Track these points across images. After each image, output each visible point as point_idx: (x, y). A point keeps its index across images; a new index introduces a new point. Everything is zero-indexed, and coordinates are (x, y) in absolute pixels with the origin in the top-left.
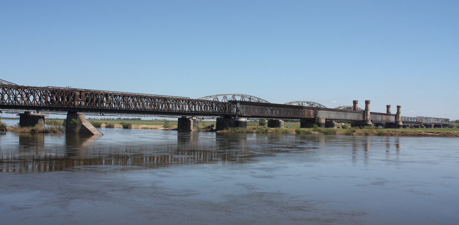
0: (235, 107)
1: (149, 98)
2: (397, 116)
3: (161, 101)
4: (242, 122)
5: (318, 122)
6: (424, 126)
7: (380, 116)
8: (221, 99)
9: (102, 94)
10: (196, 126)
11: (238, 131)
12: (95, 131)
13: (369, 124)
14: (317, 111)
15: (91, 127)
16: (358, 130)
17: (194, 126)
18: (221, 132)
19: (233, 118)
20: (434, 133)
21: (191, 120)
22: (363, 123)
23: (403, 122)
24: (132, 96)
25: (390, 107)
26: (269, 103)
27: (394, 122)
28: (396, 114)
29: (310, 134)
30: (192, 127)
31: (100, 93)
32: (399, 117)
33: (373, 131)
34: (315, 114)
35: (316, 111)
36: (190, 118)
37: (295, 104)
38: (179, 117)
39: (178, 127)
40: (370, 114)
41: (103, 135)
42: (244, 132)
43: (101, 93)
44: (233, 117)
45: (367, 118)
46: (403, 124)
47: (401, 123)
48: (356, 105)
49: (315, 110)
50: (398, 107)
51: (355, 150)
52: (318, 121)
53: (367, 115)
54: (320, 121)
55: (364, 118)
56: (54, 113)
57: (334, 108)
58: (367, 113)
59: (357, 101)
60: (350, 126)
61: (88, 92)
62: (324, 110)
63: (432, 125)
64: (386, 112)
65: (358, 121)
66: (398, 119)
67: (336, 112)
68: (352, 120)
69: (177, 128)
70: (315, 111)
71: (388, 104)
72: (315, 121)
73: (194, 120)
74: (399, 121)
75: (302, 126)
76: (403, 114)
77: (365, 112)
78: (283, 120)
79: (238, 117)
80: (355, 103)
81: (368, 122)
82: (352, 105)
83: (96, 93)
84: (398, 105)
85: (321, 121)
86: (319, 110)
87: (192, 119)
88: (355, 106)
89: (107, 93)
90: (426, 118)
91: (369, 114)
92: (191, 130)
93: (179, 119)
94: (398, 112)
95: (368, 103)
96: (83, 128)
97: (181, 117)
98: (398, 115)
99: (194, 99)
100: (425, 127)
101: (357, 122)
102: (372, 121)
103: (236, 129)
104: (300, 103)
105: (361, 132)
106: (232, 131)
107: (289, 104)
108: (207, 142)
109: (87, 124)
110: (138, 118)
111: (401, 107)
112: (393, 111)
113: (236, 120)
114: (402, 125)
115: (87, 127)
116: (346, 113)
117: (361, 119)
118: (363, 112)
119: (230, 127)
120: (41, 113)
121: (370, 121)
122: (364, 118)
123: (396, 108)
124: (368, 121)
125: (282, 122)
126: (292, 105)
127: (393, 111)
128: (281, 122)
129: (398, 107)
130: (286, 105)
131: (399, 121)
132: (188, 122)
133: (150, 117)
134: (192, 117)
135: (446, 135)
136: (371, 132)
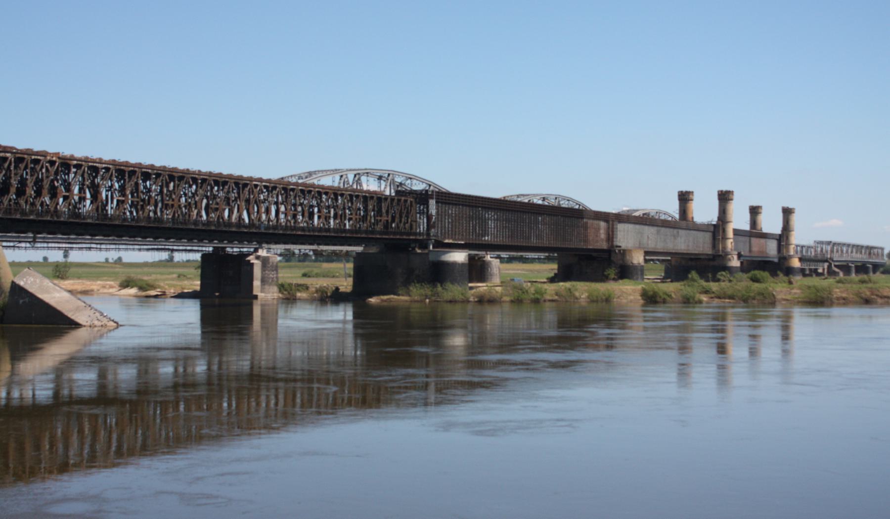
0: (423, 213)
1: (320, 193)
2: (783, 238)
3: (268, 197)
4: (454, 264)
5: (621, 262)
6: (837, 270)
7: (747, 239)
8: (370, 185)
9: (52, 163)
10: (270, 280)
11: (447, 296)
12: (78, 309)
13: (732, 267)
14: (615, 226)
15: (57, 295)
16: (694, 286)
17: (263, 281)
18: (383, 301)
19: (419, 251)
21: (251, 259)
22: (711, 263)
23: (801, 260)
24: (147, 173)
25: (760, 210)
26: (445, 193)
27: (776, 260)
28: (780, 235)
29: (696, 303)
30: (257, 283)
31: (45, 156)
32: (788, 244)
33: (881, 290)
34: (611, 236)
35: (613, 225)
36: (249, 254)
37: (327, 181)
38: (204, 249)
39: (202, 285)
40: (735, 234)
41: (118, 325)
42: (469, 302)
43: (48, 158)
44: (419, 248)
45: (724, 248)
46: (802, 266)
47: (796, 263)
48: (689, 205)
49: (611, 223)
50: (787, 212)
51: (684, 348)
52: (623, 260)
53: (725, 238)
54: (628, 257)
55: (714, 246)
56: (57, 245)
57: (614, 212)
58: (724, 231)
59: (693, 192)
60: (663, 271)
61: (8, 155)
62: (630, 223)
63: (851, 267)
65: (693, 257)
66: (788, 250)
67: (656, 228)
68: (676, 254)
69: (198, 288)
70: (611, 226)
72: (612, 258)
73: (265, 261)
74: (791, 257)
75: (564, 275)
76: (801, 237)
77: (718, 230)
78: (498, 257)
79: (433, 247)
80: (685, 198)
81: (730, 260)
83: (33, 157)
84: (786, 205)
85: (632, 257)
86: (620, 222)
87: (258, 258)
88: (684, 211)
89: (67, 159)
90: (858, 246)
91: (730, 234)
92: (256, 297)
93: (205, 257)
94: (787, 228)
95: (689, 200)
96: (21, 301)
97: (211, 249)
98: (788, 238)
99: (265, 177)
100: (841, 274)
101: (691, 259)
102: (739, 256)
103: (439, 289)
104: (351, 177)
105: (844, 295)
106: (426, 299)
107: (300, 177)
108: (313, 340)
109: (38, 281)
110: (157, 259)
112: (771, 224)
113: (432, 258)
114: (798, 268)
115: (40, 296)
116: (675, 231)
118: (712, 229)
119: (418, 282)
120: (288, 256)
121: (735, 257)
122: (782, 252)
124: (730, 256)
125: (493, 263)
126: (316, 182)
127: (771, 224)
128: (490, 262)
129: (787, 212)
130: (507, 201)
131: (791, 257)
132: (241, 265)
133: (137, 253)
134: (256, 250)
136: (878, 293)
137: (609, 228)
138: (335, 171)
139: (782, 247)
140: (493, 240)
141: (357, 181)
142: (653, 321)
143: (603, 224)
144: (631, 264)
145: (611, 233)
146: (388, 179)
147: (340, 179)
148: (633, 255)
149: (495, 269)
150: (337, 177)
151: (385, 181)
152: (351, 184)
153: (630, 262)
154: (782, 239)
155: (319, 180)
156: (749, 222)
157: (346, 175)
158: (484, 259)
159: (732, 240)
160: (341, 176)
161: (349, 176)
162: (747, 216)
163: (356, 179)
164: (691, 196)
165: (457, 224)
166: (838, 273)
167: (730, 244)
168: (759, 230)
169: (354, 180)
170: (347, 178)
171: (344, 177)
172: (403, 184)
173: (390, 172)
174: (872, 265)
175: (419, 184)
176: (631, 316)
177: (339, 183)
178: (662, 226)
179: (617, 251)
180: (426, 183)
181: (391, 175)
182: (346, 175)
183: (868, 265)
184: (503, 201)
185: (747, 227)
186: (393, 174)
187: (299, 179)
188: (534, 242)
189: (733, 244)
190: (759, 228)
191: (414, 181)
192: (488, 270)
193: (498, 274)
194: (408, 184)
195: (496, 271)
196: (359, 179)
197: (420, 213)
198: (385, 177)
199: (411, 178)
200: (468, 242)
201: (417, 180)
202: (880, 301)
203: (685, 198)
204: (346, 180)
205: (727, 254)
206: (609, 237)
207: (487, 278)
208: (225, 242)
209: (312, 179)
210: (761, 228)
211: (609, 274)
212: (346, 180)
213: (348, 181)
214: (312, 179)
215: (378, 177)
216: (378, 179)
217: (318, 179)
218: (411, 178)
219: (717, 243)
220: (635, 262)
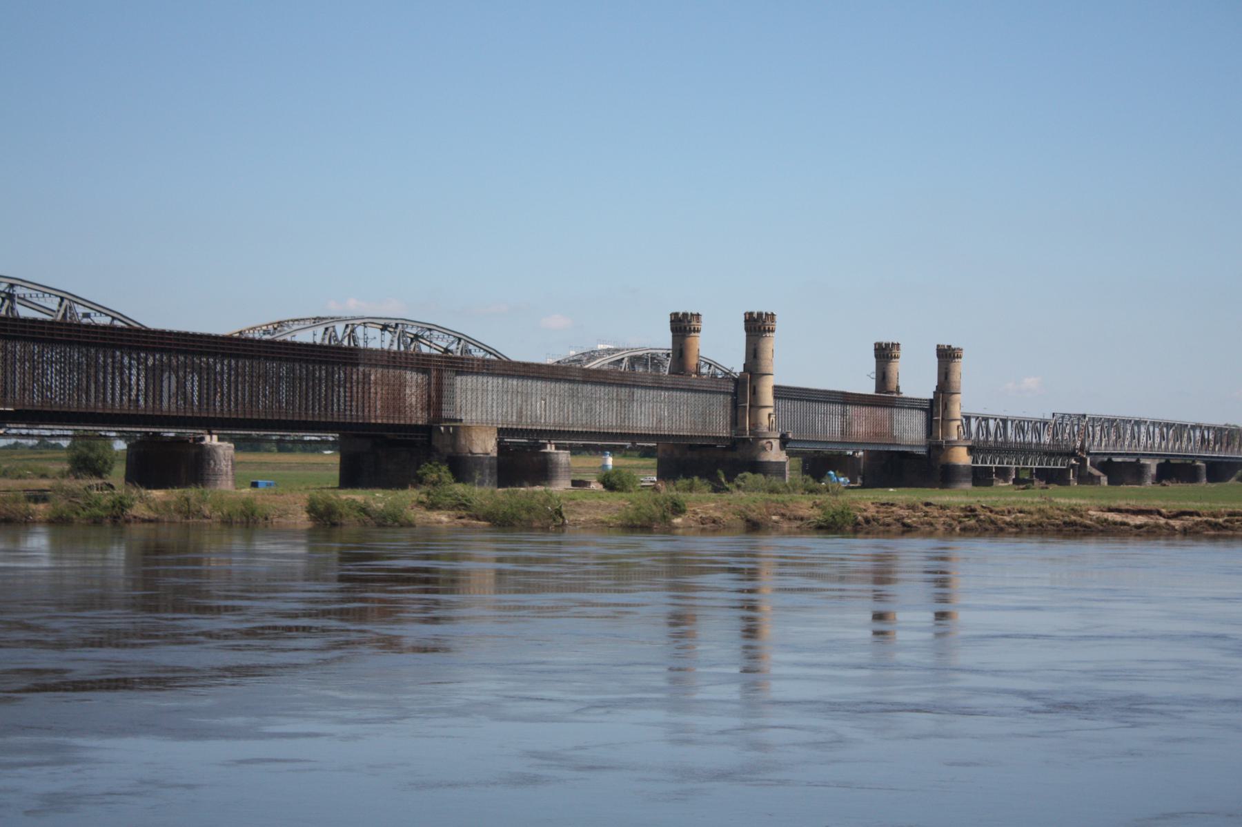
5: (450, 450)
6: (1096, 472)
7: (838, 408)
13: (769, 462)
14: (446, 381)
20: (1160, 513)
23: (971, 450)
26: (138, 330)
27: (922, 451)
28: (931, 401)
29: (402, 526)
32: (947, 420)
33: (791, 505)
34: (435, 400)
45: (755, 425)
47: (962, 457)
49: (434, 373)
50: (947, 356)
53: (756, 406)
54: (463, 442)
55: (735, 422)
58: (755, 392)
60: (655, 472)
62: (493, 375)
63: (1144, 466)
64: (868, 387)
66: (947, 432)
70: (433, 381)
71: (885, 339)
72: (433, 443)
74: (951, 445)
80: (683, 326)
81: (764, 449)
82: (662, 340)
86: (459, 373)
91: (768, 397)
94: (945, 388)
95: (892, 357)
102: (784, 441)
104: (340, 328)
105: (717, 514)
111: (964, 354)
116: (624, 392)
117: (720, 427)
118: (731, 387)
121: (776, 443)
122: (934, 434)
123: (933, 362)
125: (221, 451)
128: (213, 449)
129: (947, 356)
130: (247, 340)
135: (1226, 528)
137: (429, 384)
138: (317, 320)
139: (934, 423)
140: (173, 407)
141: (349, 335)
142: (529, 572)
143: (413, 379)
144: (469, 455)
145: (433, 394)
146: (395, 332)
147: (325, 333)
148: (474, 434)
149: (224, 463)
150: (321, 330)
151: (390, 332)
152: (340, 338)
153: (467, 451)
154: (935, 410)
155: (294, 336)
156: (874, 376)
157: (334, 327)
158: (203, 443)
159: (771, 410)
160: (327, 329)
161: (337, 328)
162: (870, 364)
163: (348, 331)
164: (694, 323)
165: (342, 390)
166: (1099, 477)
167: (765, 417)
168: (892, 392)
169: (345, 332)
170: (334, 331)
171: (331, 329)
172: (420, 337)
173: (398, 322)
174: (1204, 462)
175: (95, 314)
176: (46, 522)
177: (323, 339)
178: (585, 382)
179: (442, 428)
180: (454, 336)
181: (400, 326)
182: (334, 327)
183: (1198, 463)
184: (237, 339)
185: (868, 387)
186: (403, 324)
187: (264, 334)
188: (313, 415)
189: (773, 418)
190: (892, 387)
191: (435, 333)
192: (209, 464)
193: (230, 473)
194: (428, 336)
195: (227, 466)
196: (353, 331)
197: (52, 362)
198: (391, 327)
199: (430, 330)
200: (19, 408)
201: (439, 331)
202: (785, 525)
203: (683, 326)
204: (333, 334)
205: (758, 437)
206: (429, 401)
207: (208, 480)
208: (151, 433)
209: (284, 334)
210: (898, 387)
211: (425, 474)
212: (333, 334)
213: (336, 336)
214: (284, 334)
215: (381, 327)
216: (382, 330)
217: (292, 334)
218: (430, 330)
219: (740, 414)
220: (478, 449)
